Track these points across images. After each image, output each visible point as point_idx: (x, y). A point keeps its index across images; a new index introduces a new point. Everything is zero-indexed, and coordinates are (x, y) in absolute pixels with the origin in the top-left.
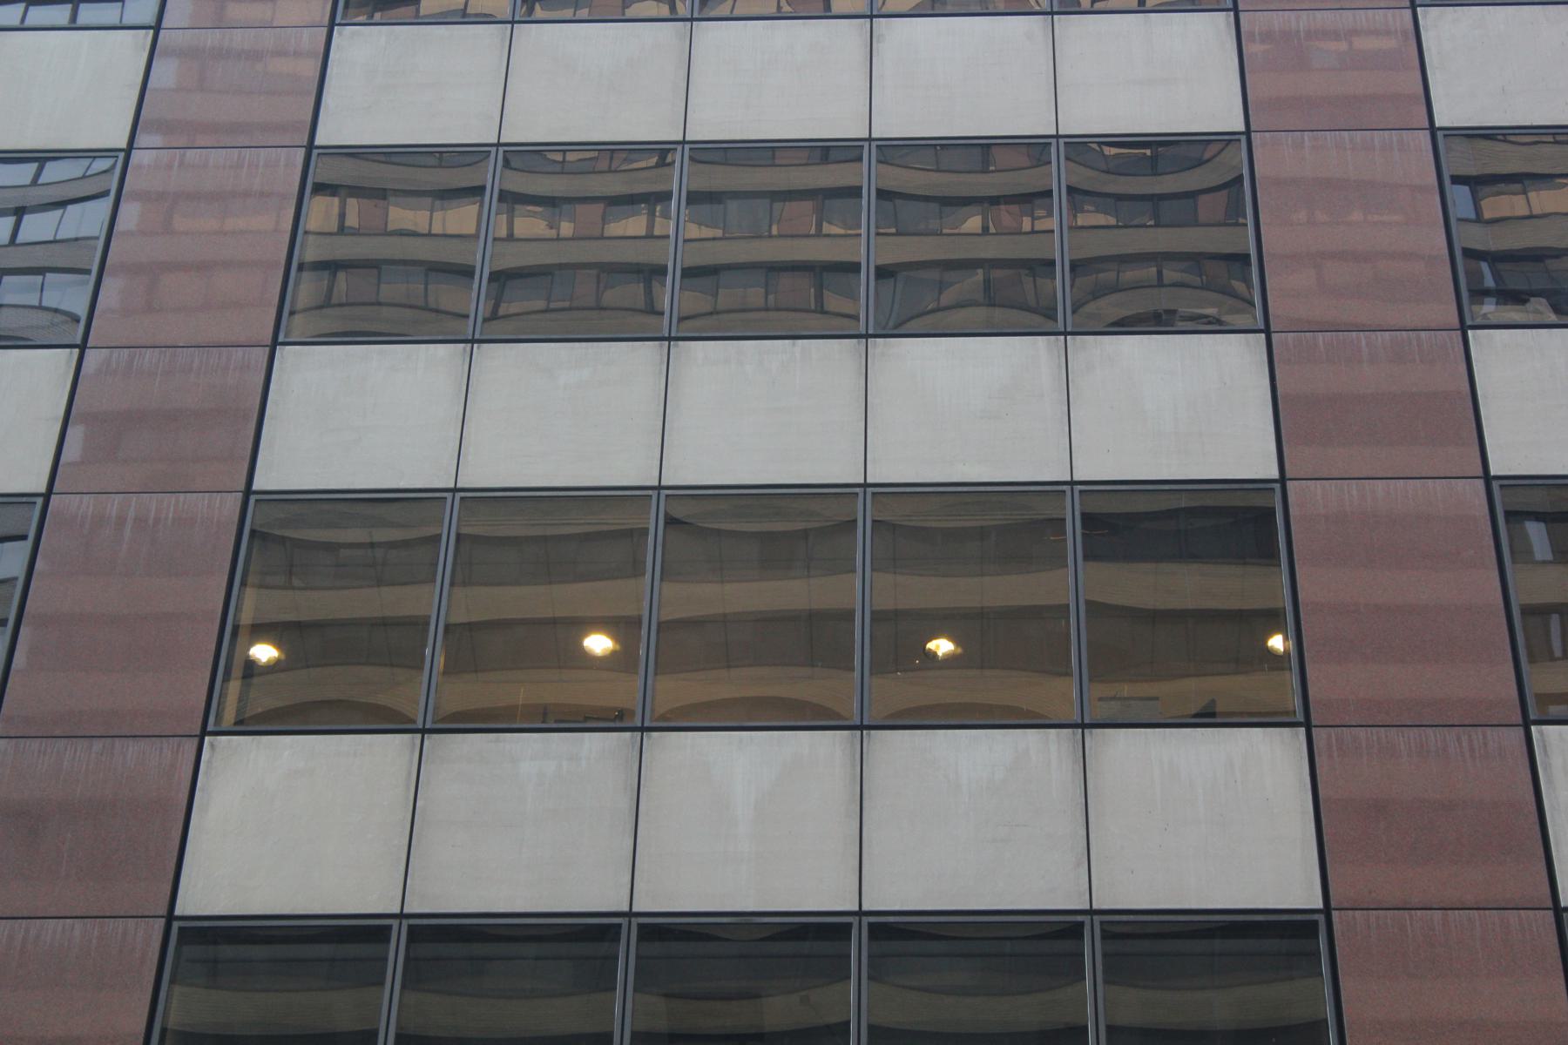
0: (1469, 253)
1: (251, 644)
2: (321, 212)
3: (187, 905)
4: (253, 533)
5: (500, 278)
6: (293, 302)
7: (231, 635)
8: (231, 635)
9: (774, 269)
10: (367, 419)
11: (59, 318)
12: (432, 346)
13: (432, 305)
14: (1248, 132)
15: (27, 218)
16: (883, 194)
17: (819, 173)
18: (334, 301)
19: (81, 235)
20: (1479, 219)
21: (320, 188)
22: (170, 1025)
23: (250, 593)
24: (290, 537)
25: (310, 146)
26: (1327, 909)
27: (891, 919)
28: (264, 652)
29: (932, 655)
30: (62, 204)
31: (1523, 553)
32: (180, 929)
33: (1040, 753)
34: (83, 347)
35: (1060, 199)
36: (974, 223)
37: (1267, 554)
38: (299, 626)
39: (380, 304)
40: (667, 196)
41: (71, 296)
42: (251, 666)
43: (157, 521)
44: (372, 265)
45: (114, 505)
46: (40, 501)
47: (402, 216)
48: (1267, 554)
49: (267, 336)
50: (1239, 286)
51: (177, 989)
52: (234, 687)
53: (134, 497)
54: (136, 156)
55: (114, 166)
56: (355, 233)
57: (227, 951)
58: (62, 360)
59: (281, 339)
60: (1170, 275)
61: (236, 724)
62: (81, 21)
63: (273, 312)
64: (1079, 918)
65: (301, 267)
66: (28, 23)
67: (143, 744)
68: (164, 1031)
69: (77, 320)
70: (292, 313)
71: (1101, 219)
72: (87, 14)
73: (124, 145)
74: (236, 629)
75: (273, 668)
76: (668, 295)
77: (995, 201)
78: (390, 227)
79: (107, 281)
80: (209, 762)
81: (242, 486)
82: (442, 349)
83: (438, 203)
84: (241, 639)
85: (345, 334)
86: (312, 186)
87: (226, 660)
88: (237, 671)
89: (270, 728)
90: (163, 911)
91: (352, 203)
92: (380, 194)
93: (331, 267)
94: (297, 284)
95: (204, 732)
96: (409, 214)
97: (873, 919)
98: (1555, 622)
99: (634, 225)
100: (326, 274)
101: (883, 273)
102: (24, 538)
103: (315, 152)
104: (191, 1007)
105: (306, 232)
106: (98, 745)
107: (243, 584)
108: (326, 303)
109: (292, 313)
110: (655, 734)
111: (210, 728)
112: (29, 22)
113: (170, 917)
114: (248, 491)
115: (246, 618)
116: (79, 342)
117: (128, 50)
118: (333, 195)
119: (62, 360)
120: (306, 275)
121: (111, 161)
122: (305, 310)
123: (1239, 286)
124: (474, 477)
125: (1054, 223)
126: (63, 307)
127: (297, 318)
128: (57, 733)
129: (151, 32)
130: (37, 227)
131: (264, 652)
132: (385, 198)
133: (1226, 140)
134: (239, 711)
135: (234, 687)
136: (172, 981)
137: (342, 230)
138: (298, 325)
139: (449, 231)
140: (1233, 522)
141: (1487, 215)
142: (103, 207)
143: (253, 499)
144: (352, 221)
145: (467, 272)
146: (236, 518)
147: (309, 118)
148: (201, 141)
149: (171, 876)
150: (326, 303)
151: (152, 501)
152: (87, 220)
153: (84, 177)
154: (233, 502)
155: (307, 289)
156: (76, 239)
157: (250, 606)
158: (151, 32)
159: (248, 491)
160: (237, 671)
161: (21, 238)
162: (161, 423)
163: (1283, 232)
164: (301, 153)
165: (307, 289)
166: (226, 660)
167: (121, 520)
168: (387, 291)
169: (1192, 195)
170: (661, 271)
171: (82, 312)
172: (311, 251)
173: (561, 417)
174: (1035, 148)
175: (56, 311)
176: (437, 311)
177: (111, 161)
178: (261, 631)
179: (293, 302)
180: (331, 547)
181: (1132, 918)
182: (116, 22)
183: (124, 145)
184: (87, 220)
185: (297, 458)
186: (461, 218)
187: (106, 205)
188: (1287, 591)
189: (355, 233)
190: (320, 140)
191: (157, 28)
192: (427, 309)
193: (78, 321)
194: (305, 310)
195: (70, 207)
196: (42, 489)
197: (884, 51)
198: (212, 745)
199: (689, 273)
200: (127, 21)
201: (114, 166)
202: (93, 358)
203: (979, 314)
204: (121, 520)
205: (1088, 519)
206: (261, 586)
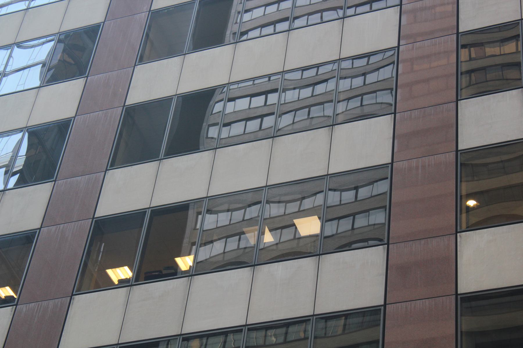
1: (467, 201)
2: (464, 54)
3: (462, 146)
4: (461, 164)
6: (461, 85)
7: (460, 199)
8: (460, 199)
11: (384, 106)
12: (510, 91)
13: (505, 78)
17: (314, 76)
18: (472, 84)
19: (386, 78)
21: (464, 46)
22: (463, 330)
23: (464, 185)
25: (458, 33)
27: (469, 295)
28: (471, 203)
30: (378, 69)
32: (461, 298)
34: (395, 113)
38: (482, 193)
39: (487, 81)
41: (386, 98)
42: (468, 208)
43: (429, 165)
44: (484, 69)
45: (414, 163)
46: (390, 165)
47: (489, 50)
49: (454, 99)
51: (463, 318)
52: (464, 216)
53: (420, 159)
54: (401, 48)
55: (395, 52)
56: (475, 59)
57: (473, 304)
58: (389, 119)
59: (459, 98)
61: (467, 228)
62: (325, 19)
63: (455, 90)
64: (378, 308)
65: (462, 74)
66: (357, 13)
67: (438, 239)
68: (461, 332)
69: (391, 105)
70: (461, 89)
72: (375, 6)
73: (397, 45)
74: (461, 196)
75: (474, 208)
78: (487, 55)
79: (399, 91)
80: (460, 242)
81: (455, 149)
82: (514, 92)
83: (501, 44)
84: (463, 200)
85: (353, 118)
86: (460, 46)
87: (460, 208)
88: (464, 210)
89: (284, 259)
90: (454, 293)
92: (481, 44)
93: (469, 72)
94: (461, 79)
95: (457, 232)
96: (493, 49)
97: (317, 317)
100: (468, 75)
102: (387, 178)
103: (460, 35)
104: (469, 323)
105: (461, 62)
106: (423, 242)
107: (461, 181)
108: (470, 85)
109: (461, 89)
110: (195, 277)
111: (458, 231)
112: (357, 12)
113: (457, 294)
114: (457, 151)
115: (464, 193)
116: (393, 111)
117: (393, 14)
118: (465, 48)
119: (389, 119)
120: (463, 76)
121: (393, 52)
122: (464, 88)
126: (383, 102)
127: (463, 91)
128: (409, 239)
129: (399, 7)
130: (371, 78)
131: (471, 203)
132: (483, 46)
134: (467, 223)
135: (464, 216)
136: (461, 315)
137: (471, 59)
138: (464, 93)
139: (506, 53)
143: (459, 153)
144: (473, 55)
146: (455, 160)
147: (456, 24)
148: (418, 40)
149: (454, 281)
150: (470, 85)
151: (426, 159)
152: (387, 73)
153: (383, 59)
154: (453, 155)
155: (464, 81)
156: (384, 80)
157: (464, 189)
158: (399, 7)
159: (457, 151)
160: (464, 210)
161: (367, 83)
162: (425, 133)
164: (455, 36)
165: (464, 81)
166: (460, 208)
167: (417, 168)
168: (489, 77)
171: (393, 103)
172: (464, 67)
175: (382, 103)
176: (507, 79)
177: (393, 52)
178: (470, 196)
179: (461, 85)
180: (485, 165)
181: (280, 322)
182: (385, 6)
183: (397, 45)
184: (387, 73)
185: (471, 137)
186: (331, 85)
189: (475, 59)
190: (461, 30)
191: (401, 5)
192: (504, 79)
193: (392, 105)
194: (466, 87)
195: (380, 70)
196: (390, 161)
198: (460, 236)
200: (388, 5)
201: (395, 52)
202: (397, 115)
204: (417, 168)
206: (467, 181)
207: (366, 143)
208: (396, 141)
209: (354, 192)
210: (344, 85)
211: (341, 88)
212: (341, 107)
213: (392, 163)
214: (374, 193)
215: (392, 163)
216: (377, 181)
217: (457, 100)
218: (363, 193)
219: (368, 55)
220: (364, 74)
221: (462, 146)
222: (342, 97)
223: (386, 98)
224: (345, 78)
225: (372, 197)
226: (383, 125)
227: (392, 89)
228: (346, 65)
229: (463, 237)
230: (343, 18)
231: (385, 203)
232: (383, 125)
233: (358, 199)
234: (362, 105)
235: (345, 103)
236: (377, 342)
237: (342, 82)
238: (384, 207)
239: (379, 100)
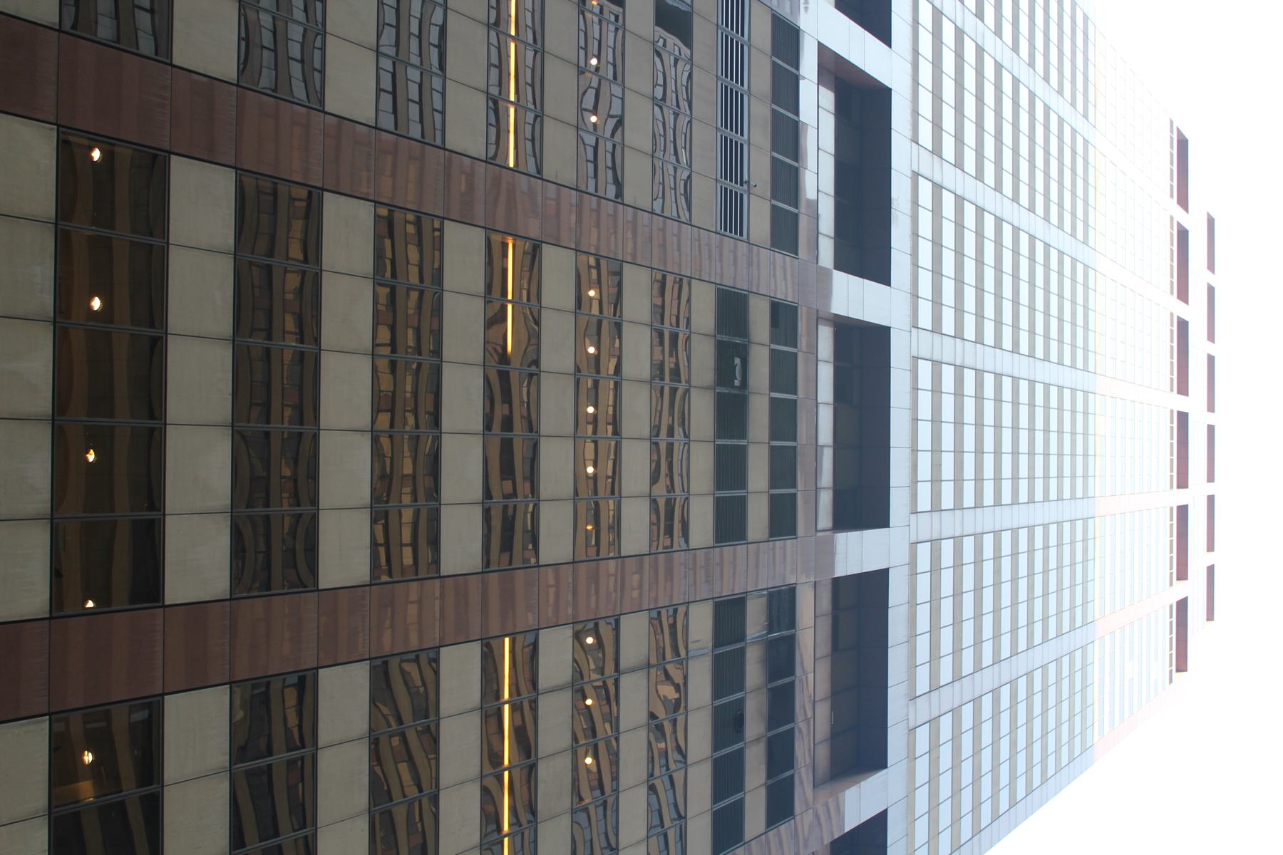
0: (268, 684)
2: (303, 193)
3: (174, 158)
4: (156, 156)
5: (269, 269)
9: (268, 385)
10: (201, 206)
14: (318, 590)
15: (148, 16)
16: (300, 434)
20: (284, 687)
21: (310, 193)
24: (153, 169)
26: (165, 606)
28: (96, 155)
29: (88, 452)
30: (305, 81)
31: (254, 687)
33: (40, 500)
34: (237, 85)
35: (297, 510)
36: (287, 472)
37: (133, 600)
40: (420, 354)
42: (91, 149)
44: (275, 212)
48: (133, 600)
50: (257, 585)
60: (261, 556)
71: (287, 525)
76: (258, 341)
77: (296, 481)
79: (304, 110)
82: (231, 241)
91: (304, 204)
93: (275, 194)
95: (59, 126)
98: (103, 724)
99: (290, 324)
101: (267, 434)
102: (156, 54)
115: (117, 149)
123: (257, 585)
124: (446, 296)
125: (286, 507)
130: (296, 69)
131: (96, 155)
133: (316, 582)
140: (148, 584)
141: (286, 691)
142: (419, 137)
145: (271, 253)
154: (166, 146)
155: (267, 185)
157: (124, 152)
159: (170, 153)
162: (206, 119)
163: (728, 551)
165: (267, 185)
169: (295, 566)
170: (269, 338)
172: (282, 188)
173: (200, 292)
174: (314, 501)
185: (335, 210)
186: (296, 251)
187: (392, 128)
188: (119, 608)
190: (326, 194)
191: (376, 128)
195: (392, 116)
197: (358, 436)
199: (268, 351)
202: (234, 88)
203: (377, 473)
205: (153, 521)
207: (352, 87)
208: (205, 79)
209: (299, 57)
210: (296, 32)
211: (292, 27)
212: (266, 20)
213: (323, 111)
214: (140, 34)
215: (323, 111)
216: (155, 40)
217: (237, 169)
218: (144, 19)
219: (322, 72)
220: (420, 103)
221: (174, 158)
222: (280, 24)
223: (266, 81)
224: (304, 36)
225: (136, 29)
226: (225, 65)
227: (275, 90)
228: (437, 83)
229: (231, 174)
230: (377, 51)
231: (123, 42)
232: (225, 65)
233: (136, 10)
234: (263, 47)
235: (271, 27)
236: (118, 42)
237: (301, 29)
238: (275, 90)
239: (264, 70)
